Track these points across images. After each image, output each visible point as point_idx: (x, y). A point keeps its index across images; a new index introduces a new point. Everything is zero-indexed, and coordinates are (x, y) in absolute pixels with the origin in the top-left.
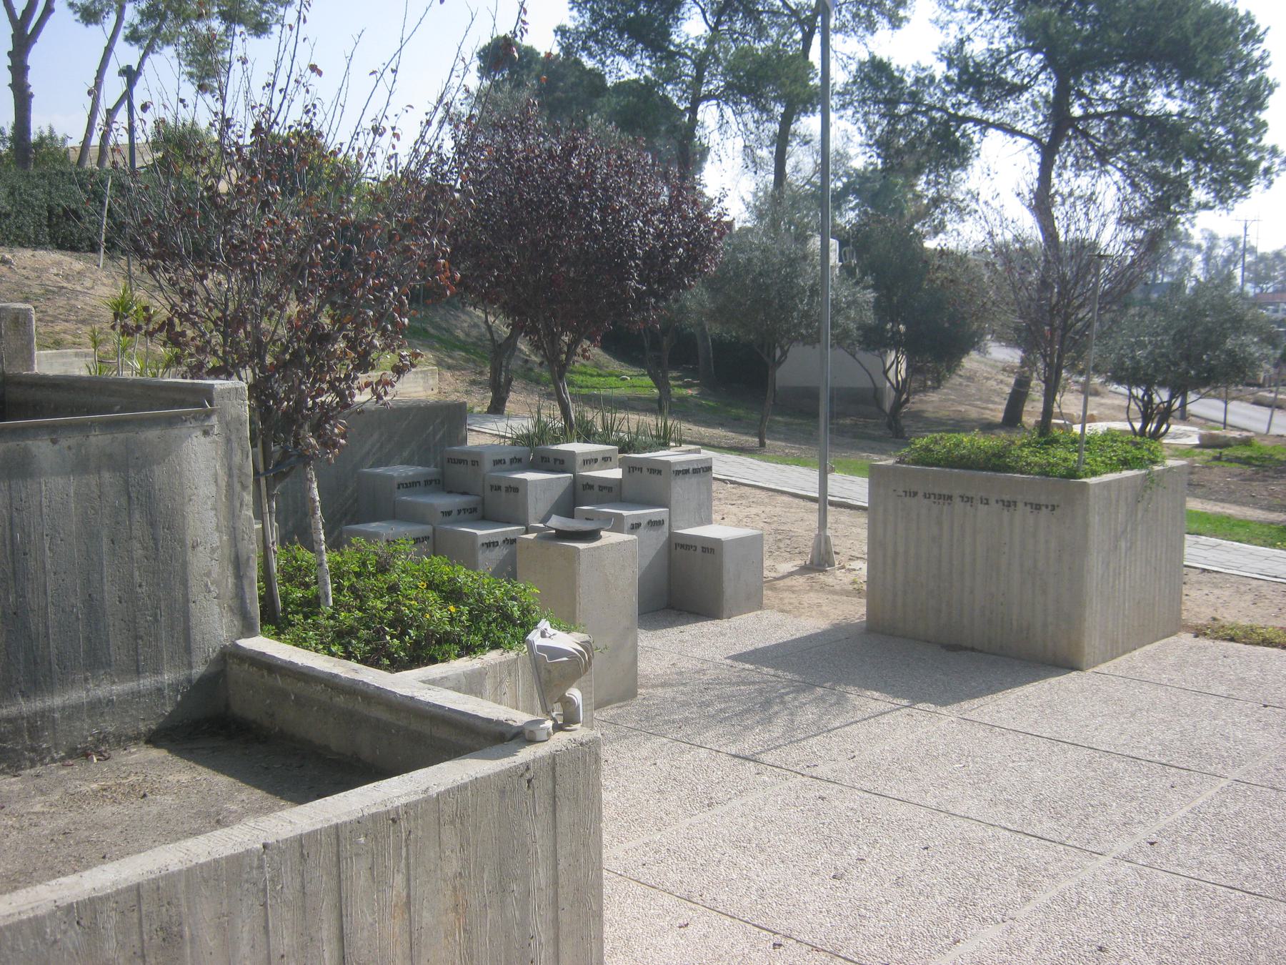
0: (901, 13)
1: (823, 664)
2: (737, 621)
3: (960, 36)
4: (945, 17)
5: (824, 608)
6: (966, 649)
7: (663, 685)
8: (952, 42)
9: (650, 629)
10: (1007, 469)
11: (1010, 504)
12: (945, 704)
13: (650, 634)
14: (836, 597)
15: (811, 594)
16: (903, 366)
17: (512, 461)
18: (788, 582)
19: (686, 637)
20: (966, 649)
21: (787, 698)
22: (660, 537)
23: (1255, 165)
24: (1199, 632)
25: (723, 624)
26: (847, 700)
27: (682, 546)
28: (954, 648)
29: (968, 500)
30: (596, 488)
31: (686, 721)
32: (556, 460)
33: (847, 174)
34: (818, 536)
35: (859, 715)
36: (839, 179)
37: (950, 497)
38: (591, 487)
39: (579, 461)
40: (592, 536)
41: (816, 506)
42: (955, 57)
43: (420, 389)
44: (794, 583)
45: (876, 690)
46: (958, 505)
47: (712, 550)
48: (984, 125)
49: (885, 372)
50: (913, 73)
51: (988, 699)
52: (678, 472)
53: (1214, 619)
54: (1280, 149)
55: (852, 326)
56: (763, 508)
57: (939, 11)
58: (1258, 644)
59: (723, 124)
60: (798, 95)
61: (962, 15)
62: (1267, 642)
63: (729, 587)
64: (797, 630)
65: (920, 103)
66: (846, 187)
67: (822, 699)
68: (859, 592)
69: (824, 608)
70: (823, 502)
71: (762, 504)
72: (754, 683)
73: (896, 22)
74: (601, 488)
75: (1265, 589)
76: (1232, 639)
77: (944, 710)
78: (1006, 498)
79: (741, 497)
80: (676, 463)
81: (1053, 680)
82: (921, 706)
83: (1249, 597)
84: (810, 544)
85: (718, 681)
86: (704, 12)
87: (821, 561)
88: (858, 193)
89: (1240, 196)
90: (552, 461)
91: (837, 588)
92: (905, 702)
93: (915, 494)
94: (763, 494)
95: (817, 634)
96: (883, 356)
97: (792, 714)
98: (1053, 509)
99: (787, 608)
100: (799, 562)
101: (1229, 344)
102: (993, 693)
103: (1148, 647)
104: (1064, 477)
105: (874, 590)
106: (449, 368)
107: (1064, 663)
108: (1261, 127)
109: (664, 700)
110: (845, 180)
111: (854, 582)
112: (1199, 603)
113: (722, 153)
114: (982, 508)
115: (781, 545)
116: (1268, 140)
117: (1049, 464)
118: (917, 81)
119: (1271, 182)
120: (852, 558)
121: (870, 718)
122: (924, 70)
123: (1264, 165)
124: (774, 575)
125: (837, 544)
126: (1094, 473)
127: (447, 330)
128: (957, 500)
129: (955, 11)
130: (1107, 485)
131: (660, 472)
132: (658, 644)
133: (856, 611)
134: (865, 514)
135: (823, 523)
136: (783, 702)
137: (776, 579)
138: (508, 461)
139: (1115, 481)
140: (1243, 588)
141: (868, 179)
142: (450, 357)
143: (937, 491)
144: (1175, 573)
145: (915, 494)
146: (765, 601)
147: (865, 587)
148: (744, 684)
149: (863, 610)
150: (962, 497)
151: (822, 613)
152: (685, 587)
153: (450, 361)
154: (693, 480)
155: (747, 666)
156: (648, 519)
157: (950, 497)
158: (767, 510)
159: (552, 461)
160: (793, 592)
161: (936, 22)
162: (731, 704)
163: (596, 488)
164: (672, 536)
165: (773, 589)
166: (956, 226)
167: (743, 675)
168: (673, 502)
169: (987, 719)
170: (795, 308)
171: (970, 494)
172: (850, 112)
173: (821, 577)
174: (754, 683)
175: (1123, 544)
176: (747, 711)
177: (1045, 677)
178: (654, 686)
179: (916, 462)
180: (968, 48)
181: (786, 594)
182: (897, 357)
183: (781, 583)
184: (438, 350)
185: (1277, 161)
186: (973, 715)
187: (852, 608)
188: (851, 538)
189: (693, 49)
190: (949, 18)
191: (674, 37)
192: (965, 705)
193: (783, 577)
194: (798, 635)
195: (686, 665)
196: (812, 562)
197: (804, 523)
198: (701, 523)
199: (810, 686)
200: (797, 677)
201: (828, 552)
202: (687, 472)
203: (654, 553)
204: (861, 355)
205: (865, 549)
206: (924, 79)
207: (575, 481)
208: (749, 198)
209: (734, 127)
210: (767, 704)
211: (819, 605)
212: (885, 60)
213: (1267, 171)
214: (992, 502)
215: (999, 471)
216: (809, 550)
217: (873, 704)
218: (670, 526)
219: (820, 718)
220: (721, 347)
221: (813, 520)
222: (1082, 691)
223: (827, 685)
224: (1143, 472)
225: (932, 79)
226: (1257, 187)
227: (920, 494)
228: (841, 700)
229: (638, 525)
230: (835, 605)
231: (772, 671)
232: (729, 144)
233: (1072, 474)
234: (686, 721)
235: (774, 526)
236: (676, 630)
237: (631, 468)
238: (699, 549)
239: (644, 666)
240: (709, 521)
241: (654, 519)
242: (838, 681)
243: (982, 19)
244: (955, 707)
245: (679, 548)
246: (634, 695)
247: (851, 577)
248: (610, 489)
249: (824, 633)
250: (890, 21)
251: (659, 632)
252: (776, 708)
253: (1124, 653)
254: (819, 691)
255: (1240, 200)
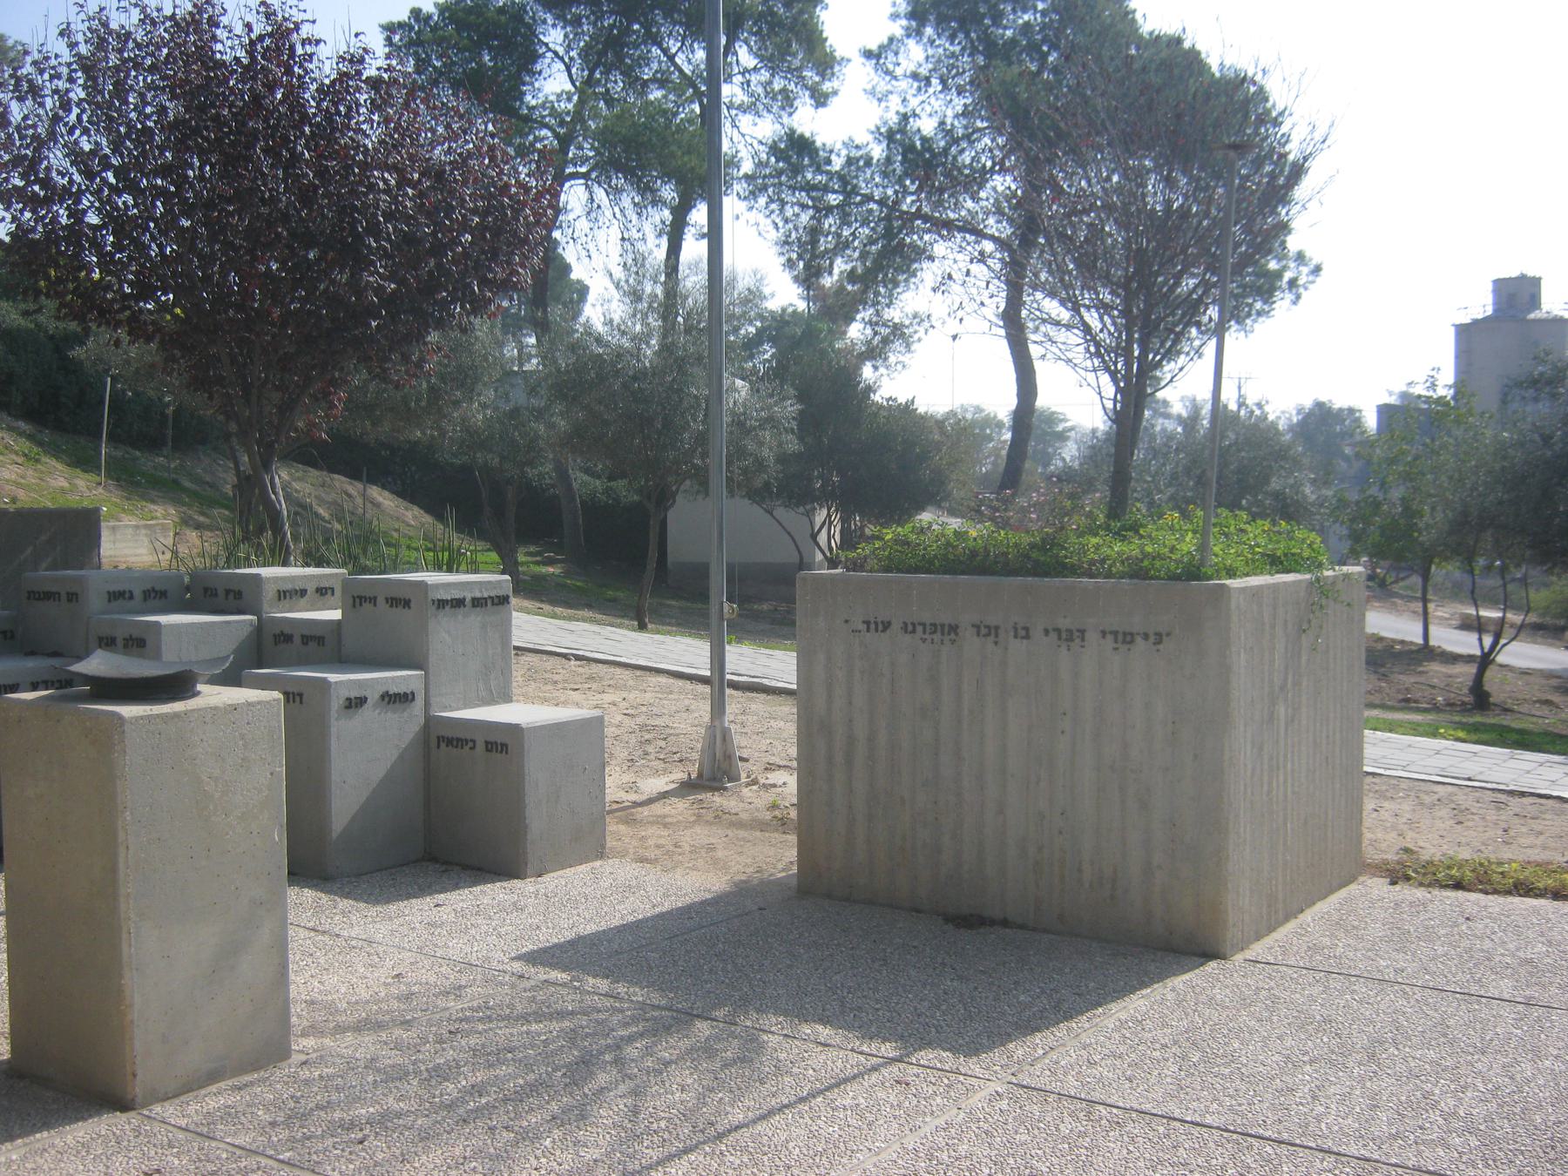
0: (827, 86)
1: (707, 967)
2: (552, 881)
3: (902, 110)
4: (883, 85)
5: (720, 854)
6: (992, 922)
7: (358, 1028)
8: (893, 119)
9: (377, 902)
10: (1062, 569)
11: (1071, 636)
12: (973, 1049)
13: (373, 911)
14: (742, 833)
15: (698, 829)
16: (837, 531)
17: (147, 594)
18: (657, 809)
19: (445, 914)
20: (992, 922)
21: (632, 1051)
22: (409, 723)
23: (1278, 275)
24: (1396, 875)
25: (526, 886)
26: (762, 1046)
27: (450, 742)
28: (971, 921)
29: (989, 631)
30: (297, 640)
31: (383, 1122)
32: (228, 592)
33: (761, 317)
34: (711, 728)
35: (788, 1088)
36: (751, 323)
37: (954, 629)
38: (288, 638)
39: (269, 592)
40: (175, 686)
41: (707, 689)
42: (897, 135)
43: (143, 551)
44: (667, 810)
45: (824, 1021)
46: (971, 644)
47: (504, 748)
48: (945, 227)
49: (814, 536)
50: (844, 152)
51: (1061, 1031)
52: (441, 604)
53: (1407, 850)
54: (1308, 254)
55: (766, 452)
56: (625, 695)
57: (876, 79)
58: (1509, 893)
59: (592, 209)
60: (693, 169)
61: (903, 84)
62: (1523, 889)
63: (537, 819)
64: (666, 896)
65: (855, 190)
66: (760, 332)
67: (707, 1050)
68: (782, 823)
69: (720, 854)
70: (718, 683)
71: (624, 687)
72: (561, 1015)
73: (820, 99)
74: (306, 639)
75: (1462, 799)
76: (1458, 886)
77: (973, 1066)
78: (1064, 623)
79: (591, 678)
80: (437, 586)
81: (1179, 981)
82: (926, 1056)
83: (1444, 812)
84: (699, 746)
85: (488, 1014)
86: (568, 69)
87: (715, 772)
88: (773, 340)
89: (1259, 314)
90: (221, 592)
91: (744, 816)
92: (888, 1049)
93: (887, 626)
94: (627, 673)
95: (704, 903)
96: (810, 515)
97: (635, 1093)
98: (1159, 642)
99: (651, 854)
100: (679, 775)
101: (1275, 484)
102: (1068, 1017)
103: (1321, 907)
104: (1176, 578)
105: (810, 821)
106: (198, 526)
107: (1191, 946)
108: (1284, 228)
109: (351, 1063)
110: (758, 324)
111: (774, 806)
112: (1382, 832)
113: (591, 246)
114: (1017, 647)
115: (650, 749)
116: (1293, 243)
117: (1146, 555)
118: (850, 161)
119: (1298, 297)
120: (770, 767)
121: (813, 1095)
122: (857, 147)
123: (1287, 276)
124: (633, 797)
125: (743, 743)
126: (1231, 573)
127: (211, 485)
128: (968, 634)
129: (895, 78)
130: (1256, 592)
131: (407, 603)
132: (380, 931)
133: (779, 857)
134: (791, 700)
135: (718, 708)
136: (618, 1062)
137: (636, 804)
138: (137, 593)
139: (1269, 586)
140: (1427, 799)
141: (788, 323)
142: (203, 514)
143: (927, 617)
144: (1351, 778)
145: (887, 626)
146: (610, 842)
147: (793, 814)
148: (539, 1017)
149: (792, 854)
150: (977, 627)
151: (715, 861)
152: (451, 821)
153: (202, 519)
154: (473, 620)
155: (556, 975)
156: (382, 689)
157: (954, 629)
158: (631, 696)
159: (221, 592)
160: (665, 826)
161: (872, 92)
162: (502, 1071)
163: (297, 640)
164: (430, 722)
165: (630, 821)
166: (901, 358)
167: (540, 996)
168: (433, 659)
169: (1071, 1085)
170: (686, 427)
171: (992, 620)
172: (762, 200)
173: (717, 799)
174: (561, 1015)
175: (1281, 710)
176: (533, 1088)
177: (1161, 977)
178: (340, 1029)
179: (887, 570)
180: (914, 124)
181: (651, 830)
182: (829, 516)
183: (645, 812)
184: (184, 504)
185: (1305, 270)
186: (1037, 1076)
187: (772, 852)
188: (769, 740)
189: (554, 113)
190: (889, 87)
191: (528, 98)
192: (1018, 1049)
193: (650, 801)
194: (666, 907)
195: (427, 975)
196: (700, 775)
197: (689, 715)
198: (490, 701)
199: (683, 1019)
200: (656, 998)
201: (728, 757)
202: (458, 603)
203: (395, 754)
204: (780, 512)
205: (793, 752)
206: (858, 160)
207: (259, 629)
208: (619, 273)
209: (608, 213)
210: (585, 1065)
211: (711, 848)
212: (807, 135)
213: (1293, 283)
214: (1037, 633)
215: (1046, 574)
216: (696, 756)
217: (818, 1058)
218: (427, 704)
219: (701, 1099)
220: (593, 509)
221: (704, 709)
222: (1245, 1003)
223: (719, 1014)
224: (1308, 576)
225: (868, 163)
226: (1282, 302)
227: (896, 626)
228: (752, 1046)
229: (361, 701)
230: (738, 850)
231: (603, 985)
232: (601, 235)
233: (1193, 572)
234: (383, 1122)
235: (639, 720)
236: (428, 901)
237: (357, 600)
238: (480, 747)
239: (304, 983)
240: (506, 697)
241: (393, 690)
242: (743, 1004)
243: (931, 90)
244: (997, 1055)
245: (443, 741)
246: (283, 1053)
247: (769, 797)
248: (320, 640)
249: (718, 901)
250: (812, 97)
251: (393, 908)
252: (602, 1078)
253: (1287, 919)
254: (703, 1029)
255: (1261, 319)
